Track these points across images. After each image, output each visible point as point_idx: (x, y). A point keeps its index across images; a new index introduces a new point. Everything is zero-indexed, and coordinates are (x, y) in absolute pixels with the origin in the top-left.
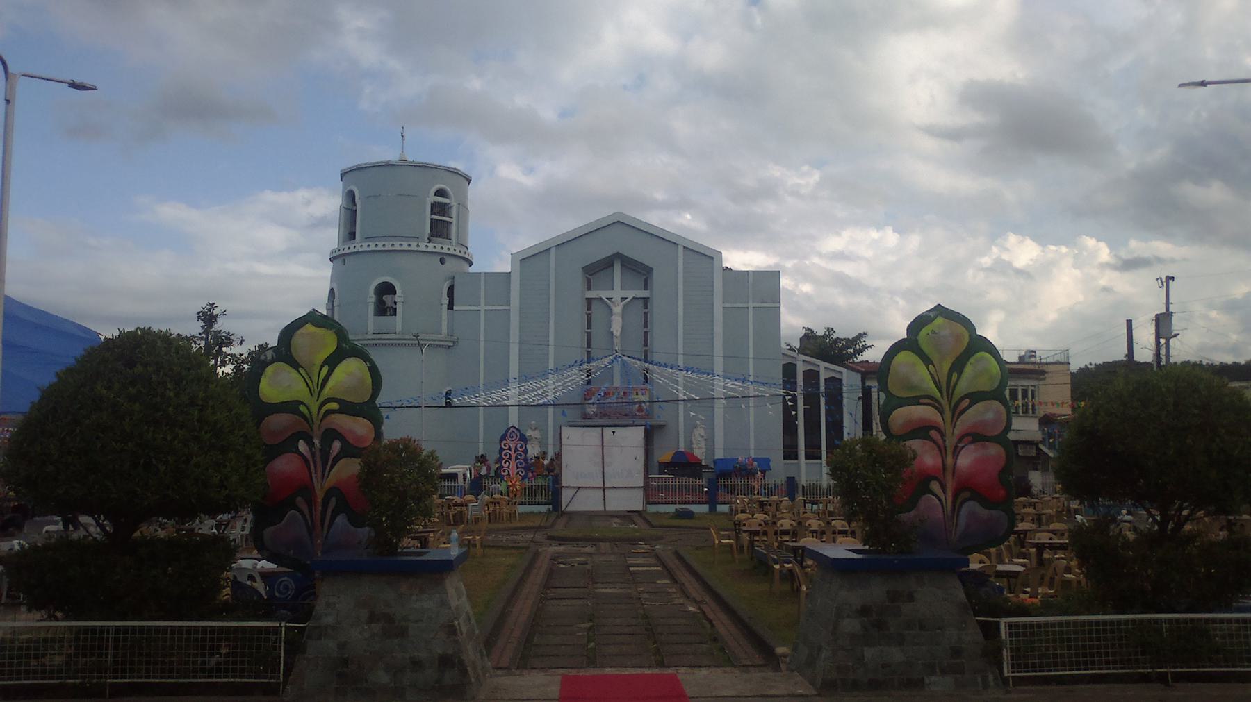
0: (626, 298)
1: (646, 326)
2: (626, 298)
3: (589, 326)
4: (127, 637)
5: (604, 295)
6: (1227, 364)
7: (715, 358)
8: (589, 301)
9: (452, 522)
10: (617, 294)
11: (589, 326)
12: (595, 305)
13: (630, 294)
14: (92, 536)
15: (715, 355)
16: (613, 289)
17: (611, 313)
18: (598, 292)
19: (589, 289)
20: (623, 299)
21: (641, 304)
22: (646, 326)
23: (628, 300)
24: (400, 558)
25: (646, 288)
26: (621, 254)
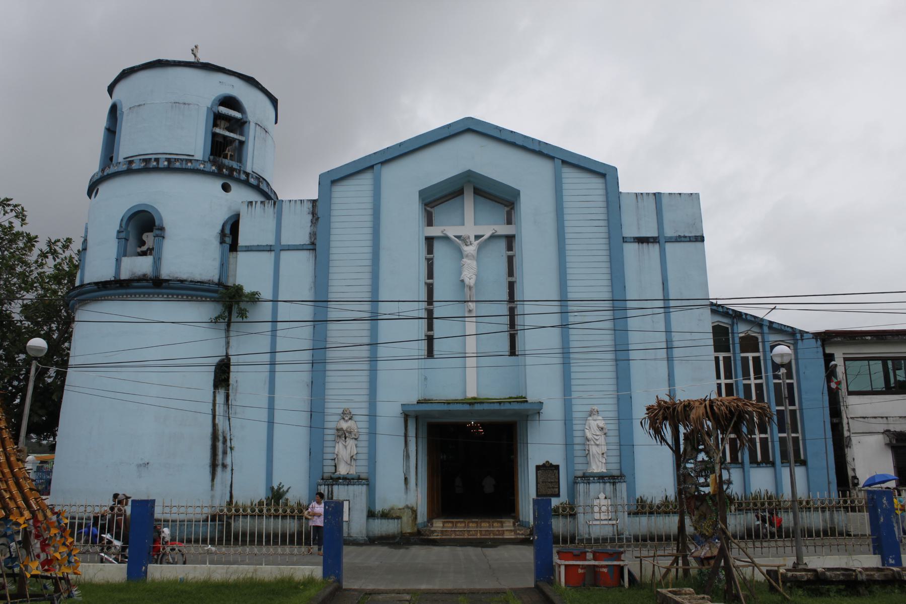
0: (483, 236)
1: (511, 273)
2: (483, 236)
3: (430, 275)
4: (160, 547)
5: (451, 232)
6: (389, 535)
7: (275, 424)
8: (430, 241)
9: (89, 560)
10: (469, 229)
11: (430, 275)
12: (438, 247)
13: (487, 231)
14: (652, 242)
15: (275, 422)
16: (463, 224)
17: (461, 254)
18: (442, 228)
19: (430, 223)
20: (477, 237)
21: (503, 244)
22: (511, 273)
23: (485, 237)
24: (59, 582)
25: (509, 222)
26: (421, 190)
